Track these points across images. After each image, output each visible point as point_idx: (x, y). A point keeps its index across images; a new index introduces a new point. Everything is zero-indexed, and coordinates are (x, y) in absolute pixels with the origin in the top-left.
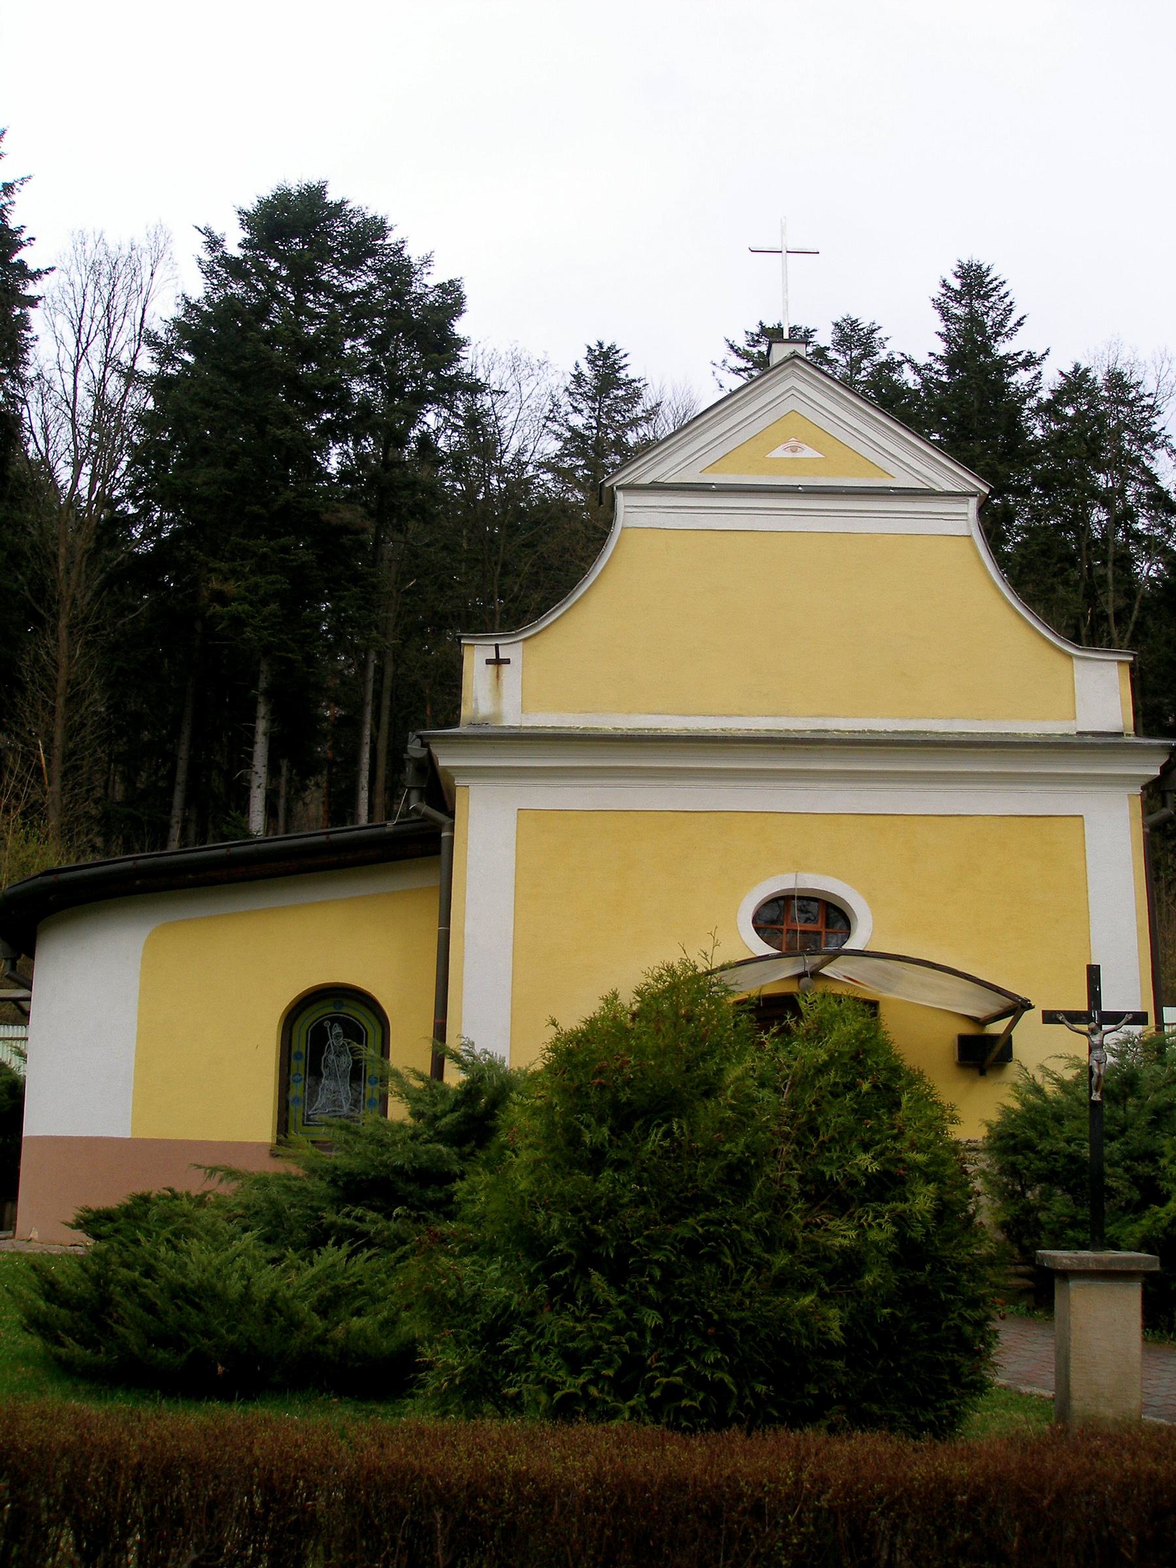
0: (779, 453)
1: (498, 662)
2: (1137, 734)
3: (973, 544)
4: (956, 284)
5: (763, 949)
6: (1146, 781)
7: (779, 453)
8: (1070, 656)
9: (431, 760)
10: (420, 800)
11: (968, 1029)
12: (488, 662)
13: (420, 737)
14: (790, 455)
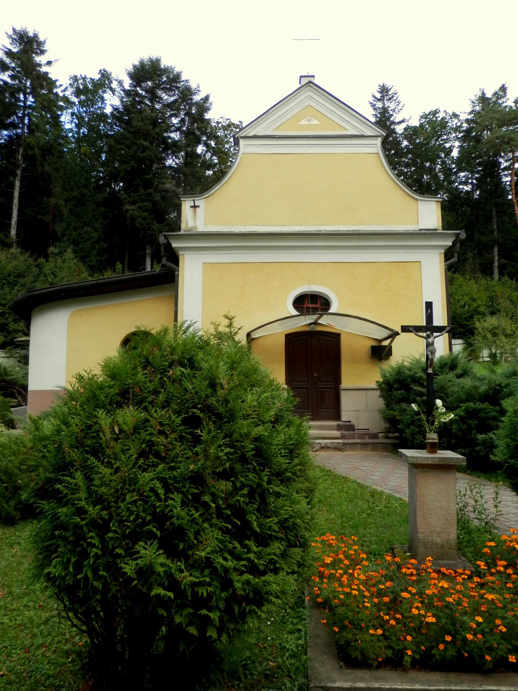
0: (303, 122)
1: (195, 207)
2: (443, 229)
3: (379, 156)
4: (378, 96)
5: (295, 312)
6: (447, 247)
7: (303, 122)
8: (417, 200)
9: (170, 245)
10: (167, 260)
11: (374, 344)
12: (191, 207)
13: (164, 235)
14: (307, 123)
